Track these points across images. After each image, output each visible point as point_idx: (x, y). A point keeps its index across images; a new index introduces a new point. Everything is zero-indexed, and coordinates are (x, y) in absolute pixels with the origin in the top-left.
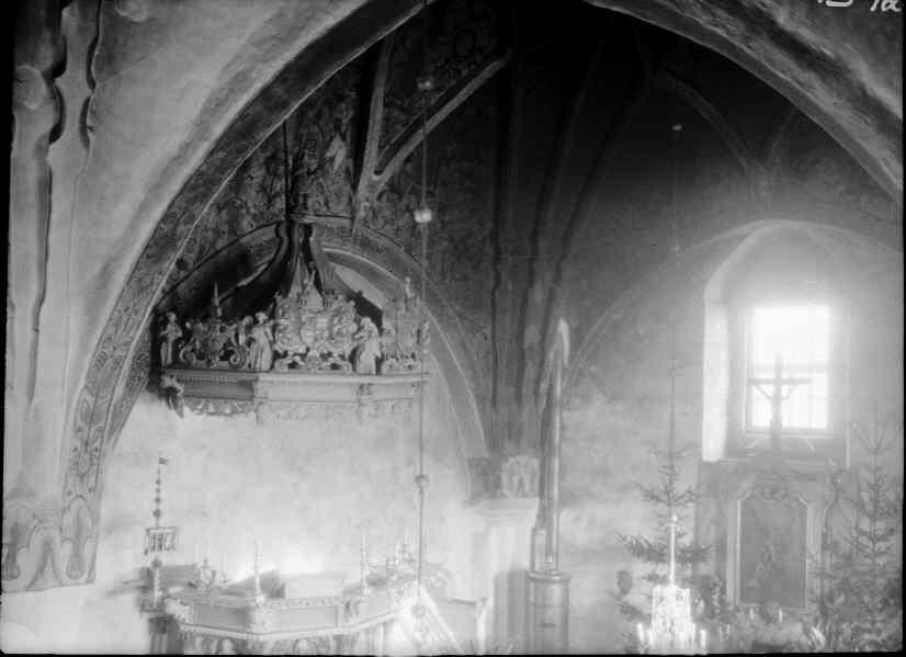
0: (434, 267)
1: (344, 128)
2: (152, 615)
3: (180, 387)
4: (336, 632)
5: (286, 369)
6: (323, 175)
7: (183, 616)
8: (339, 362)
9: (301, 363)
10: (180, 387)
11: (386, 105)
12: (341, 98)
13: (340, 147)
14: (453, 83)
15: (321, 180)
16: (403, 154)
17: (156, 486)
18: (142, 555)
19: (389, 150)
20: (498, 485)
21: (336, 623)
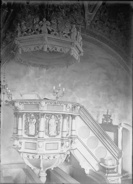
5: (23, 36)
9: (26, 34)
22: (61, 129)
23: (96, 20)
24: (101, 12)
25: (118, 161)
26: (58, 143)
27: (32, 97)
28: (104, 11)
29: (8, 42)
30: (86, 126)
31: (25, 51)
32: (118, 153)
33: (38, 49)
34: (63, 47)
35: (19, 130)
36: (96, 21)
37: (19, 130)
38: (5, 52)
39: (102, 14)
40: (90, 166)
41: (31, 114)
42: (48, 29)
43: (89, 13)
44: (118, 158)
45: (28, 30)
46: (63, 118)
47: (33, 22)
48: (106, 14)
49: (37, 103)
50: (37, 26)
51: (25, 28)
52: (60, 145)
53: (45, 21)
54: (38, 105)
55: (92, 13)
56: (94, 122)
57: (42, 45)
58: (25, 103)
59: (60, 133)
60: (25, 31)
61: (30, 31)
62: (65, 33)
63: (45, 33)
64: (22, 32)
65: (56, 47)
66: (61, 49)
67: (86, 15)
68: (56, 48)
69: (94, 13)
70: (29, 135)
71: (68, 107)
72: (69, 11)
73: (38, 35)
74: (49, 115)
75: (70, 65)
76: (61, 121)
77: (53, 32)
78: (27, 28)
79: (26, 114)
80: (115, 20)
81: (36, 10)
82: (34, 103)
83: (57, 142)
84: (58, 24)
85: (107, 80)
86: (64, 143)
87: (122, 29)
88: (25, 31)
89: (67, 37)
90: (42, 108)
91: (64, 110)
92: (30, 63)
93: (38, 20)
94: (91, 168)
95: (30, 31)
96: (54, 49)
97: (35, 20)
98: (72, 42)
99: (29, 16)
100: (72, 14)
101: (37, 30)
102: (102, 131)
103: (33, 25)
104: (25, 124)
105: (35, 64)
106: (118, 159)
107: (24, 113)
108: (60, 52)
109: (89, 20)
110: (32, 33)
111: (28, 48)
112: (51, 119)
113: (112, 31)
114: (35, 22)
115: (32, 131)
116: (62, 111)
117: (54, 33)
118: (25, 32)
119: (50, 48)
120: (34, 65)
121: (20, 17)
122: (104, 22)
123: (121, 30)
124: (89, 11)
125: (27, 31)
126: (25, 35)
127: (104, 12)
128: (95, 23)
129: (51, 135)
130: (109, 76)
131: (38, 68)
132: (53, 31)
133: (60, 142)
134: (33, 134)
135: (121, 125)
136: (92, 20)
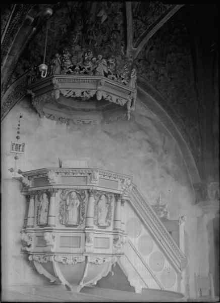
0: (168, 97)
1: (119, 29)
2: (25, 194)
3: (33, 94)
4: (86, 187)
5: (66, 73)
6: (110, 44)
7: (28, 184)
8: (88, 71)
9: (72, 72)
10: (33, 94)
11: (134, 18)
12: (116, 15)
13: (104, 14)
14: (164, 12)
15: (109, 45)
16: (145, 41)
17: (18, 127)
18: (15, 160)
19: (137, 38)
20: (206, 194)
21: (87, 183)
22: (112, 218)
23: (139, 58)
24: (146, 49)
25: (181, 274)
26: (108, 238)
27: (82, 164)
28: (150, 46)
29: (20, 76)
30: (136, 217)
31: (66, 95)
32: (180, 261)
33: (87, 96)
34: (119, 97)
35: (51, 216)
36: (139, 61)
37: (51, 216)
38: (13, 90)
39: (147, 51)
40: (144, 283)
41: (71, 191)
42: (104, 71)
43: (133, 48)
44: (180, 269)
45: (74, 67)
46: (117, 200)
47: (83, 57)
48: (152, 51)
49: (88, 174)
50: (90, 65)
51: (69, 63)
52: (111, 241)
53: (100, 59)
54: (87, 177)
55: (136, 49)
56: (150, 212)
57: (94, 90)
58: (64, 174)
59: (112, 223)
60: (70, 68)
61: (77, 68)
62: (123, 79)
63: (100, 75)
64: (62, 68)
65: (74, 91)
66: (82, 93)
67: (128, 50)
68: (74, 93)
69: (140, 49)
70: (67, 225)
71: (125, 183)
72: (105, 40)
73: (90, 77)
74: (99, 194)
75: (109, 122)
76: (113, 204)
77: (110, 75)
78: (72, 64)
79: (63, 192)
80: (164, 63)
81: (62, 31)
82: (79, 175)
83: (106, 236)
84: (116, 65)
85: (150, 151)
86: (118, 239)
87: (172, 77)
88: (70, 68)
89: (125, 84)
90: (94, 182)
91: (119, 188)
92: (44, 113)
93: (91, 55)
94: (144, 286)
95: (77, 68)
96: (71, 94)
97: (86, 55)
98: (131, 92)
99: (78, 48)
100: (109, 45)
101: (89, 69)
102: (159, 223)
103: (84, 61)
104: (61, 208)
105: (51, 115)
106: (180, 271)
107: (58, 189)
108: (115, 103)
109: (131, 57)
110: (81, 72)
111: (70, 91)
112: (100, 201)
113: (159, 79)
114: (86, 58)
115: (73, 217)
116: (116, 189)
117: (112, 76)
118: (70, 70)
119: (65, 94)
120: (50, 117)
121: (39, 39)
122: (149, 63)
123: (171, 79)
124: (133, 45)
125: (73, 68)
126: (69, 73)
127: (151, 49)
128: (137, 63)
129: (101, 225)
130: (153, 147)
131: (55, 122)
132: (109, 73)
133: (111, 237)
134: (75, 224)
135: (183, 218)
136: (135, 58)
